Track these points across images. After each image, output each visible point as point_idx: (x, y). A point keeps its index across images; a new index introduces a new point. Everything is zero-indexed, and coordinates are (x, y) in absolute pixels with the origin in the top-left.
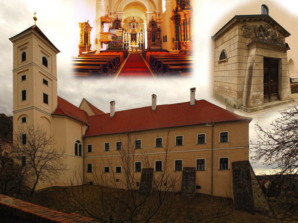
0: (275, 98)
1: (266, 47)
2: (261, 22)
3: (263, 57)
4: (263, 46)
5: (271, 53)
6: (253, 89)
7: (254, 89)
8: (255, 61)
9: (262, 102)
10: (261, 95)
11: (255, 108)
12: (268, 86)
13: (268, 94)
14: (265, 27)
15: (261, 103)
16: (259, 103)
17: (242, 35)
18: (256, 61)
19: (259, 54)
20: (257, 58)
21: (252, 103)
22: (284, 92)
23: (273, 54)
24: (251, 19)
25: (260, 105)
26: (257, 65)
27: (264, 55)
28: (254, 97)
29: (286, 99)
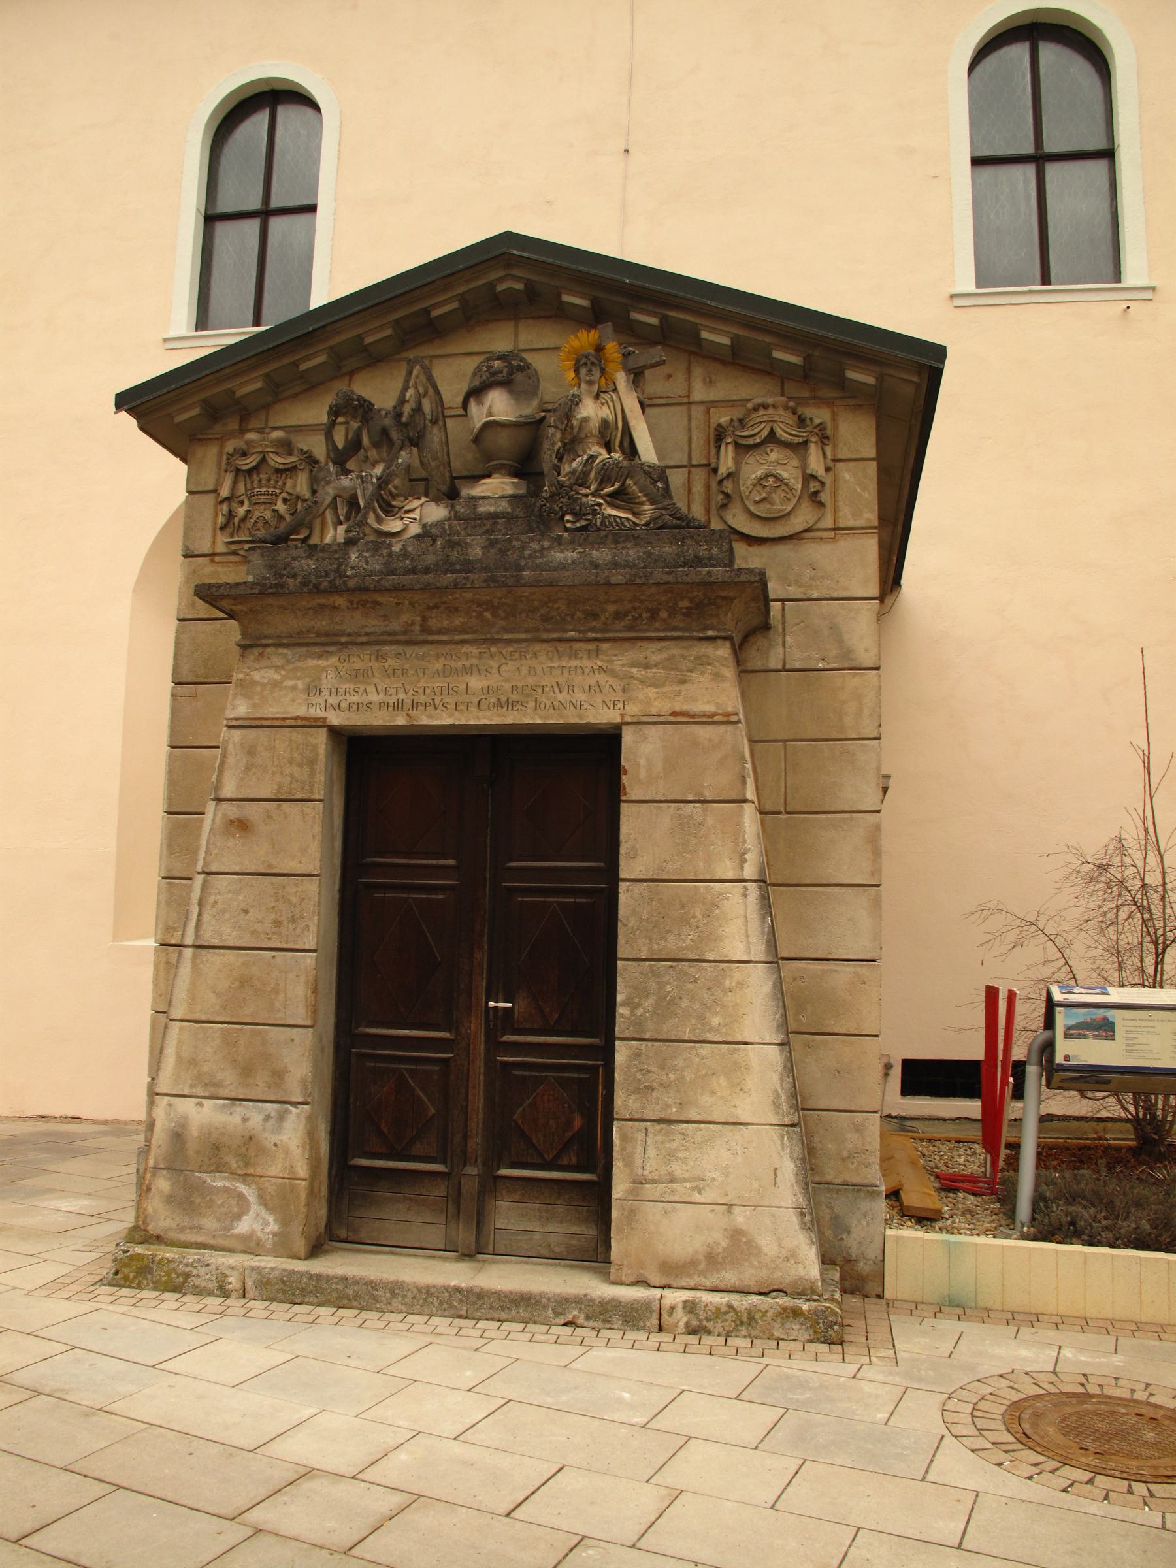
0: (575, 1229)
1: (374, 624)
2: (450, 349)
3: (321, 738)
4: (323, 623)
5: (443, 673)
6: (179, 1059)
7: (193, 1062)
8: (217, 787)
9: (285, 1222)
10: (269, 1138)
11: (169, 1253)
12: (446, 1062)
13: (444, 1162)
14: (410, 393)
15: (273, 1226)
16: (244, 1226)
17: (221, 548)
18: (228, 790)
19: (272, 710)
20: (251, 751)
21: (170, 1199)
22: (652, 1165)
23: (476, 683)
24: (360, 338)
25: (250, 1245)
26: (242, 826)
27: (335, 719)
28: (192, 1147)
29: (673, 1272)
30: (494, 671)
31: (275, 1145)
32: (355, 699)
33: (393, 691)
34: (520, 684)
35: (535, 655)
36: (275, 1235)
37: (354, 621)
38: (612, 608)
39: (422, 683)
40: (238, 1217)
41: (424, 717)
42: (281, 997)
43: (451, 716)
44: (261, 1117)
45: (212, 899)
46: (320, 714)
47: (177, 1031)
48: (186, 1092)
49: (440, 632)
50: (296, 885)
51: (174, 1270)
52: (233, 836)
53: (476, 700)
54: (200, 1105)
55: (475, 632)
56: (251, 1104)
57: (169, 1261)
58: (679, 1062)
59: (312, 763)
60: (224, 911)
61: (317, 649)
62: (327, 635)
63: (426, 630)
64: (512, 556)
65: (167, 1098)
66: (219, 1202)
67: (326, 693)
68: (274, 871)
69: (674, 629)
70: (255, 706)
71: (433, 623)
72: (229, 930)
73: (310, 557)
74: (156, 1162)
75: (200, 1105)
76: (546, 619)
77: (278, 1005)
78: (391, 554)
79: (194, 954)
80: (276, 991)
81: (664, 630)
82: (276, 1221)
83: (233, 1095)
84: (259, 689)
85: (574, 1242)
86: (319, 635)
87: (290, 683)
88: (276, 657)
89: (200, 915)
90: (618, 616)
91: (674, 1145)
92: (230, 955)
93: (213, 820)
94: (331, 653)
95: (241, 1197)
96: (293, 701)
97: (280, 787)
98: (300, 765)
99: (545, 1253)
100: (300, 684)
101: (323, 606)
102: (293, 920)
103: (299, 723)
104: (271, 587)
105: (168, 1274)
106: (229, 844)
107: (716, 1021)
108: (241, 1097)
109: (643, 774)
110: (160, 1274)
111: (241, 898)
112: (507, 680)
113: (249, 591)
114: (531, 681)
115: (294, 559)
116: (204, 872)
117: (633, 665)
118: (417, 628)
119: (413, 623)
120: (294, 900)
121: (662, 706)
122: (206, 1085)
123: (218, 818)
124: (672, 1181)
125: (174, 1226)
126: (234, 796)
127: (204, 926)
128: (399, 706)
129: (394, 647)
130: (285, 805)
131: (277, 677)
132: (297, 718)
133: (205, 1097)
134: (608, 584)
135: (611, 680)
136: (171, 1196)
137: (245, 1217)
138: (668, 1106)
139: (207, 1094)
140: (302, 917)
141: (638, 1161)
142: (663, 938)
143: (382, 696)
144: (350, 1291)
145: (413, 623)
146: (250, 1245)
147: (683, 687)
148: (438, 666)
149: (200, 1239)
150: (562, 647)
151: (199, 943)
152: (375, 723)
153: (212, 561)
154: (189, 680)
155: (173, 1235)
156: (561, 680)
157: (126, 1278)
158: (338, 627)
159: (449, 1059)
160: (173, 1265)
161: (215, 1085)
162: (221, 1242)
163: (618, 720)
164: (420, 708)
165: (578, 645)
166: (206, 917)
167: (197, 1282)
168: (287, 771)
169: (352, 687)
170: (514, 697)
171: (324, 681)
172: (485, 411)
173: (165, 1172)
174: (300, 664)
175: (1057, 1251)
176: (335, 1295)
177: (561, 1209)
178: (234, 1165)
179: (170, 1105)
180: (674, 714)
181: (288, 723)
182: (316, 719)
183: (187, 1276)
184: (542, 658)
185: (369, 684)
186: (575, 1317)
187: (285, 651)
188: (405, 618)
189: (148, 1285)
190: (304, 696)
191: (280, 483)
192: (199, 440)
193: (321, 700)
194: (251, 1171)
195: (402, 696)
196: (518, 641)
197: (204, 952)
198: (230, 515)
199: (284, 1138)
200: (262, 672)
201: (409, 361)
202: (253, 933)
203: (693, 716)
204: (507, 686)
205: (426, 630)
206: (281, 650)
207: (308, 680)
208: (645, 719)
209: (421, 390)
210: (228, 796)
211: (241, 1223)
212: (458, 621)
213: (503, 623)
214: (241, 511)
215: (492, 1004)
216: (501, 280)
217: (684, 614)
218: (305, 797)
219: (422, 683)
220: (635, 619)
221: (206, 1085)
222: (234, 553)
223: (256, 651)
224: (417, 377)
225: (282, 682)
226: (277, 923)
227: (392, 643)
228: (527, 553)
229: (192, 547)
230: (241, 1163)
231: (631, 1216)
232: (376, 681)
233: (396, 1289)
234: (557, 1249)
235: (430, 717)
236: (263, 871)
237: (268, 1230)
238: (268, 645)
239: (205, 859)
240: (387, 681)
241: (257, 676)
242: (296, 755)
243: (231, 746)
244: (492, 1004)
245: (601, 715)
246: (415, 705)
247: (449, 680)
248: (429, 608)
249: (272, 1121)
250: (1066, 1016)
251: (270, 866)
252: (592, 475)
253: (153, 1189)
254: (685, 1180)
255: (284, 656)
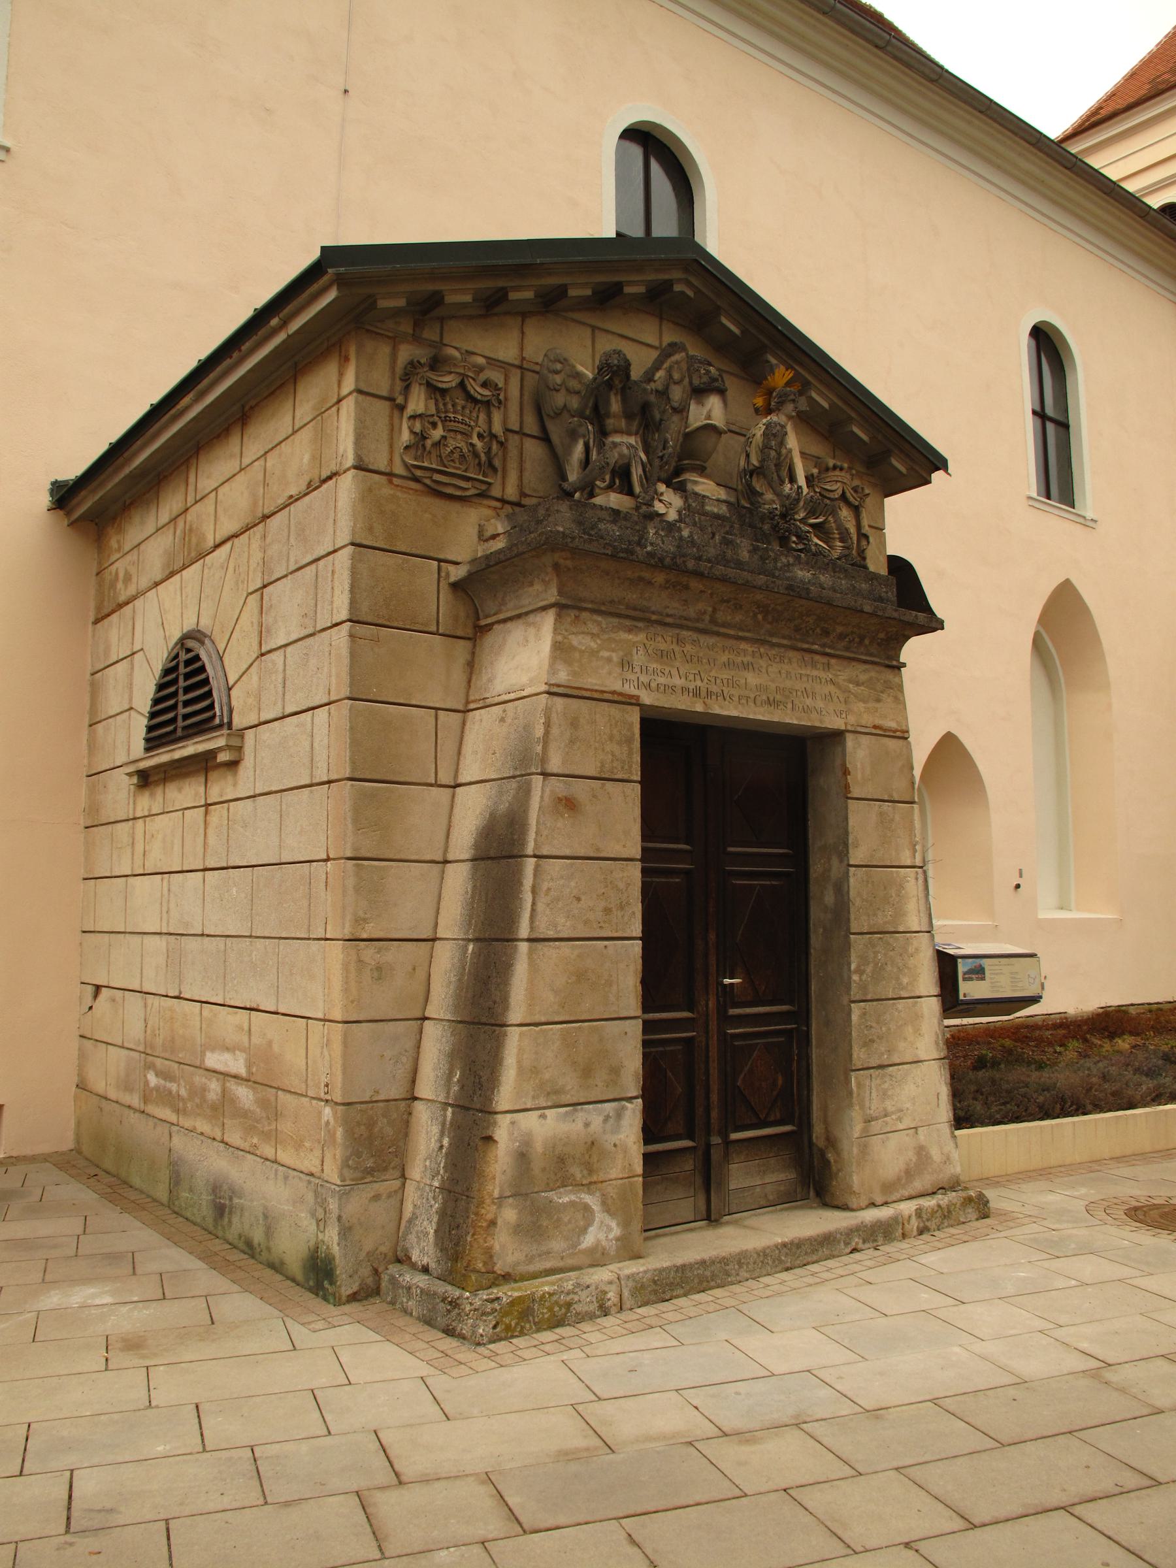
0: (782, 1176)
1: (674, 607)
5: (728, 665)
7: (535, 1071)
8: (544, 759)
9: (625, 1224)
10: (610, 1139)
11: (545, 1286)
14: (660, 374)
16: (588, 1240)
17: (399, 469)
18: (554, 765)
20: (574, 724)
23: (752, 679)
25: (598, 1257)
26: (569, 804)
27: (647, 699)
28: (537, 1166)
30: (764, 670)
31: (615, 1145)
32: (662, 680)
33: (691, 677)
34: (782, 686)
35: (790, 661)
36: (617, 1239)
37: (660, 601)
38: (839, 629)
39: (713, 673)
40: (584, 1230)
41: (716, 707)
42: (615, 987)
43: (736, 708)
44: (601, 1118)
45: (545, 886)
46: (634, 691)
47: (517, 1036)
48: (529, 1106)
49: (724, 625)
50: (622, 870)
51: (556, 1303)
52: (562, 816)
53: (752, 696)
54: (543, 1116)
55: (749, 631)
56: (591, 1106)
57: (551, 1295)
58: (887, 1017)
59: (629, 741)
60: (558, 899)
61: (628, 623)
62: (635, 609)
63: (713, 621)
64: (770, 565)
65: (509, 1116)
66: (566, 1220)
67: (637, 669)
68: (602, 855)
69: (871, 655)
70: (574, 674)
71: (721, 616)
72: (563, 920)
73: (614, 522)
74: (501, 1191)
75: (543, 1116)
76: (797, 629)
77: (612, 998)
78: (681, 538)
79: (530, 948)
80: (609, 983)
81: (866, 655)
82: (618, 1225)
83: (575, 1100)
84: (577, 655)
85: (782, 1188)
86: (628, 607)
87: (606, 654)
88: (593, 623)
89: (534, 904)
90: (841, 637)
91: (886, 1086)
92: (565, 948)
93: (542, 797)
94: (640, 629)
95: (587, 1208)
96: (610, 673)
97: (603, 766)
98: (619, 743)
99: (763, 1203)
100: (615, 657)
101: (641, 579)
102: (621, 907)
103: (616, 698)
104: (623, 551)
105: (550, 1309)
106: (559, 825)
107: (905, 980)
108: (582, 1100)
109: (859, 776)
110: (542, 1312)
111: (573, 884)
112: (773, 681)
113: (602, 551)
114: (788, 684)
115: (600, 520)
116: (535, 856)
117: (850, 681)
118: (707, 618)
119: (705, 613)
120: (621, 885)
121: (868, 720)
122: (549, 1094)
123: (546, 799)
124: (886, 1116)
125: (523, 1258)
126: (560, 771)
127: (539, 917)
128: (697, 693)
129: (690, 633)
130: (609, 784)
131: (593, 645)
132: (614, 693)
133: (545, 1108)
134: (862, 611)
135: (838, 693)
136: (518, 1226)
137: (591, 1229)
138: (883, 1054)
139: (549, 1104)
140: (628, 904)
141: (867, 1104)
142: (875, 915)
143: (683, 680)
144: (708, 1273)
145: (705, 613)
146: (598, 1257)
147: (878, 705)
148: (724, 658)
149: (548, 1265)
150: (807, 657)
151: (534, 936)
152: (679, 707)
153: (391, 482)
154: (370, 620)
155: (524, 1269)
156: (808, 687)
157: (508, 1328)
158: (645, 603)
159: (692, 1038)
160: (555, 1298)
161: (557, 1092)
162: (570, 1262)
163: (843, 728)
164: (714, 697)
165: (817, 657)
166: (540, 907)
167: (578, 1308)
168: (608, 748)
169: (659, 667)
170: (778, 697)
171: (635, 657)
172: (705, 412)
173: (511, 1200)
174: (613, 635)
175: (1041, 1127)
176: (696, 1281)
177: (772, 1161)
178: (578, 1176)
179: (513, 1123)
180: (875, 727)
181: (606, 696)
182: (632, 697)
183: (569, 1305)
184: (795, 665)
185: (673, 666)
186: (857, 1243)
187: (599, 619)
188: (701, 606)
189: (531, 1328)
190: (619, 670)
191: (475, 415)
192: (368, 331)
193: (633, 677)
194: (595, 1178)
195: (699, 683)
196: (780, 646)
197: (539, 945)
198: (422, 437)
199: (622, 1136)
200: (580, 637)
201: (797, 374)
202: (586, 922)
203: (885, 730)
204: (773, 686)
205: (713, 621)
206: (596, 617)
207: (621, 653)
208: (859, 729)
209: (676, 376)
210: (555, 771)
211: (587, 1237)
212: (738, 617)
213: (768, 626)
214: (437, 433)
215: (727, 981)
216: (679, 281)
217: (878, 644)
218: (625, 777)
219: (713, 673)
220: (850, 642)
221: (549, 1094)
222: (416, 480)
223: (573, 613)
224: (677, 362)
225: (598, 652)
226: (607, 911)
227: (688, 628)
228: (779, 565)
229: (366, 460)
230: (585, 1172)
231: (864, 1149)
232: (677, 664)
233: (741, 1259)
234: (771, 1198)
235: (721, 707)
236: (592, 855)
237: (611, 1236)
238: (586, 609)
239: (535, 840)
240: (687, 666)
241: (575, 640)
242: (615, 732)
243: (554, 715)
244: (727, 981)
245: (834, 722)
246: (709, 694)
247: (733, 673)
248: (723, 601)
249: (612, 1121)
250: (964, 965)
251: (598, 850)
252: (801, 504)
253: (499, 1221)
254: (893, 1113)
255: (599, 624)
